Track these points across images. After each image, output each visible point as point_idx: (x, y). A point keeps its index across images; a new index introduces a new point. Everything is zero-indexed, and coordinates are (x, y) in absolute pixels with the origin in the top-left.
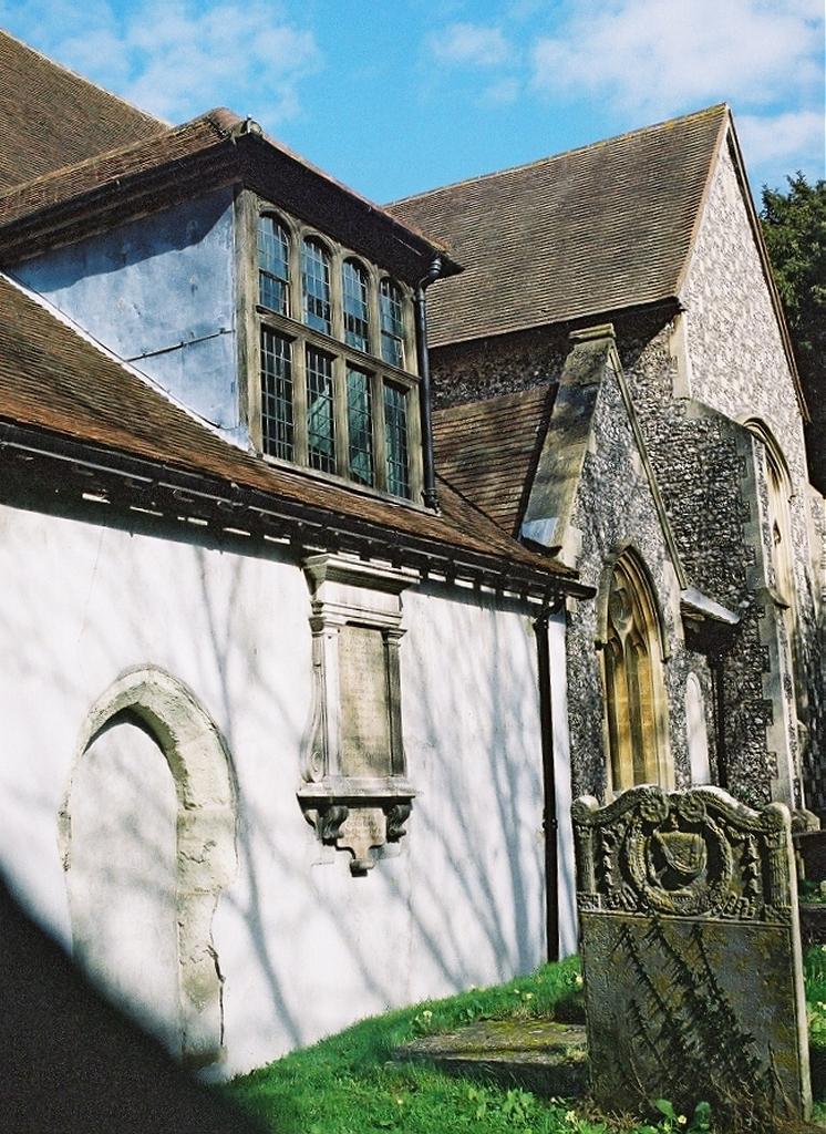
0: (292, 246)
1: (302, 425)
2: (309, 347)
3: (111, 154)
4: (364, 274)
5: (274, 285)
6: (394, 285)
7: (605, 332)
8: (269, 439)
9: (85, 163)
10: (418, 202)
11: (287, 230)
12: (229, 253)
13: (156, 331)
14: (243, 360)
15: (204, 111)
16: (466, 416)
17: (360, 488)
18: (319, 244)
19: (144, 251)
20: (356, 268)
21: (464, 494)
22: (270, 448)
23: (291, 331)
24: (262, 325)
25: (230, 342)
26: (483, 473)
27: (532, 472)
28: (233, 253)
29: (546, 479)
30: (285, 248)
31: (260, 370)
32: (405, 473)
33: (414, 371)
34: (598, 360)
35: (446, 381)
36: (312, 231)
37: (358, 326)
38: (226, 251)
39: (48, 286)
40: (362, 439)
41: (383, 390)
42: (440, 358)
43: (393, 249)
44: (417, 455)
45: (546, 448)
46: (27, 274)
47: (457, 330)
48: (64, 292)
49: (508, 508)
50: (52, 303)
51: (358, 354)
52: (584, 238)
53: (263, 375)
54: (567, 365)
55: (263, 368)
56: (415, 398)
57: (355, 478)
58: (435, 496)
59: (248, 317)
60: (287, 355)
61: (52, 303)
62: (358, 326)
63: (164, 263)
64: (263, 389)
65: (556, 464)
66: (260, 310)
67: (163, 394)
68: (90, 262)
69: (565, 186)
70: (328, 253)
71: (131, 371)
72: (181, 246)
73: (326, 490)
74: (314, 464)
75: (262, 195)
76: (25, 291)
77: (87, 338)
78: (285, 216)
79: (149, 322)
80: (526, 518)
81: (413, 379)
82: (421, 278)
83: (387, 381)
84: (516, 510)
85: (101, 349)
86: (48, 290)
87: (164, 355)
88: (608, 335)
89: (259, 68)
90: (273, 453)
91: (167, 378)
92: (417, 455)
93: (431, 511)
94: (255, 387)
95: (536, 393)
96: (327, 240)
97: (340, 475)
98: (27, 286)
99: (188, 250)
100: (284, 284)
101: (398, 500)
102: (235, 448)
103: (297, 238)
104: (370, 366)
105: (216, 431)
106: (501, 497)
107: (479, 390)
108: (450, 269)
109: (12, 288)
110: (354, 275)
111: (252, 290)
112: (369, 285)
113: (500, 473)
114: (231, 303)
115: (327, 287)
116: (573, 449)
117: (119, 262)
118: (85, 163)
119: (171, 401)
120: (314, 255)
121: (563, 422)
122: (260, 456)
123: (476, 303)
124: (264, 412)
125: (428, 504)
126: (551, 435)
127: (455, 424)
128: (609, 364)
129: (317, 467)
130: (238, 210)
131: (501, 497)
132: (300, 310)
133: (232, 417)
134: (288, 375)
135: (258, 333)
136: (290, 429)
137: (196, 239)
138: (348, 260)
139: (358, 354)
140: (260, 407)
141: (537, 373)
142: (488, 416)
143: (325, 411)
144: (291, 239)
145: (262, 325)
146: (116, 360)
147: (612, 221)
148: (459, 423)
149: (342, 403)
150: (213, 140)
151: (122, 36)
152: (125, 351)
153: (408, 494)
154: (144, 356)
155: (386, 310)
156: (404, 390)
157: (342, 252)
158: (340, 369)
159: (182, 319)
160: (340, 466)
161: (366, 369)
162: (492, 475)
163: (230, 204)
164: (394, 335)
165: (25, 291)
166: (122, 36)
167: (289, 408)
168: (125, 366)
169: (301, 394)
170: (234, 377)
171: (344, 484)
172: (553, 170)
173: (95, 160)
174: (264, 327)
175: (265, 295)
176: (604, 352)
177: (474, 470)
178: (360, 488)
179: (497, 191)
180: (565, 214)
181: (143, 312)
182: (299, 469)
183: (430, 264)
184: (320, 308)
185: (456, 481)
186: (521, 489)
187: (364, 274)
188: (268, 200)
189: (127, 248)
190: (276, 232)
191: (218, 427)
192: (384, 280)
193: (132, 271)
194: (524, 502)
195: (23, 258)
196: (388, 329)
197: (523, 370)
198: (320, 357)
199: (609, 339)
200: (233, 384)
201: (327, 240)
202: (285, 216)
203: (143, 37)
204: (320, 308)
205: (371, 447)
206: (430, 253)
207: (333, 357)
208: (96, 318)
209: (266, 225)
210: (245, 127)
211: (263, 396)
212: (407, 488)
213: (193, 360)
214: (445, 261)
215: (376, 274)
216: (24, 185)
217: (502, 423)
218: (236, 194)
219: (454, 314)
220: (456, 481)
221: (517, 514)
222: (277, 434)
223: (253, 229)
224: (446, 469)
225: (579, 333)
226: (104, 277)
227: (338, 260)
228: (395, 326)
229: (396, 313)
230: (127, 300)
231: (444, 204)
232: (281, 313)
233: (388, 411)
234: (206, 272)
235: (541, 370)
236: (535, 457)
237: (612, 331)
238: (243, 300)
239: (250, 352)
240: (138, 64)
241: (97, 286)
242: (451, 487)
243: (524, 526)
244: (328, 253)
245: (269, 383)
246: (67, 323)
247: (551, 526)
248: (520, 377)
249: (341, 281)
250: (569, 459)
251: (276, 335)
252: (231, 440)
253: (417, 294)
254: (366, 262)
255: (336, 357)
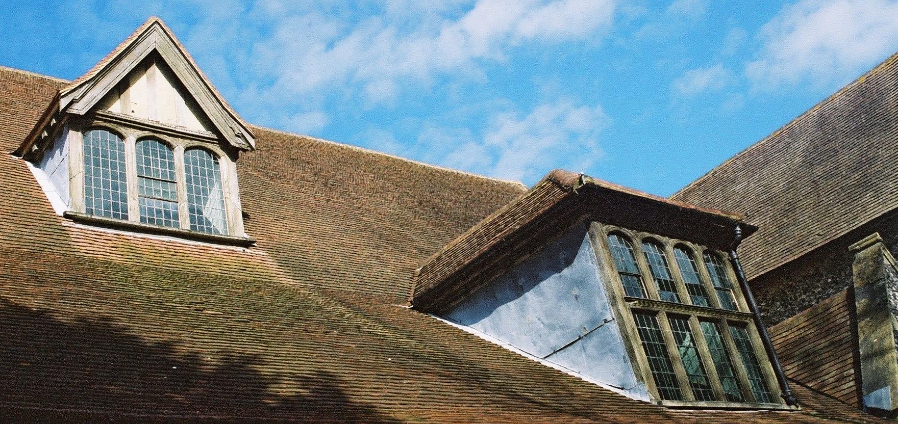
0: (635, 250)
1: (680, 370)
2: (669, 315)
3: (489, 219)
4: (690, 253)
5: (632, 280)
6: (713, 254)
7: (874, 239)
8: (661, 388)
9: (473, 229)
10: (699, 185)
11: (629, 239)
12: (596, 267)
13: (558, 332)
14: (626, 338)
15: (546, 174)
16: (792, 327)
17: (737, 405)
18: (654, 242)
19: (534, 280)
20: (683, 250)
21: (810, 385)
22: (665, 395)
23: (655, 308)
24: (632, 309)
25: (614, 327)
26: (819, 366)
27: (856, 356)
28: (596, 262)
29: (869, 357)
30: (631, 252)
31: (640, 342)
32: (763, 383)
33: (747, 310)
34: (877, 258)
35: (764, 304)
36: (647, 234)
37: (697, 290)
38: (592, 265)
39: (475, 318)
40: (725, 367)
41: (730, 331)
42: (756, 287)
43: (703, 229)
44: (768, 367)
45: (861, 337)
46: (458, 315)
47: (758, 266)
48: (486, 321)
49: (849, 385)
50: (480, 330)
51: (703, 310)
52: (829, 175)
53: (643, 344)
54: (855, 270)
55: (642, 340)
56: (753, 327)
57: (730, 399)
58: (792, 395)
59: (621, 307)
60: (656, 325)
61: (480, 330)
62: (697, 290)
63: (550, 285)
64: (647, 354)
65: (872, 346)
66: (628, 300)
67: (577, 375)
68: (499, 296)
69: (801, 145)
70: (661, 246)
71: (549, 365)
72: (559, 270)
73: (715, 415)
74: (699, 398)
75: (604, 222)
76: (460, 327)
77: (511, 349)
78: (624, 230)
79: (552, 327)
80: (865, 393)
81: (747, 315)
82: (731, 243)
83: (731, 323)
84: (854, 388)
85: (524, 354)
86: (475, 322)
87: (569, 348)
88: (878, 241)
89: (573, 135)
90: (667, 398)
91: (575, 363)
92: (768, 367)
93: (793, 407)
94: (641, 355)
95: (839, 298)
96: (657, 237)
97: (719, 399)
98: (461, 323)
99: (565, 272)
100: (637, 276)
101: (768, 406)
102: (641, 402)
103: (637, 242)
104: (717, 316)
105: (622, 393)
106: (840, 379)
107: (790, 304)
108: (749, 230)
109: (451, 327)
110: (683, 255)
111: (618, 286)
112: (695, 257)
113: (832, 363)
114: (606, 300)
115: (668, 270)
116: (880, 332)
117: (519, 291)
118: (473, 229)
119: (584, 379)
120: (652, 250)
121: (866, 313)
122: (660, 404)
123: (767, 243)
124: (652, 370)
125: (789, 404)
126: (861, 324)
127: (784, 334)
128: (886, 261)
129: (701, 399)
130: (592, 236)
131: (840, 379)
132: (653, 288)
133: (633, 380)
134: (661, 340)
135: (631, 317)
136: (674, 377)
137: (569, 262)
138: (676, 246)
139: (703, 310)
140: (648, 367)
141: (829, 280)
142: (807, 323)
143: (691, 351)
144: (633, 245)
145: (632, 309)
146: (536, 360)
147: (847, 158)
148: (787, 333)
149: (704, 347)
150: (559, 195)
151: (481, 143)
152: (540, 352)
153: (772, 399)
154: (555, 352)
155: (714, 272)
156: (745, 325)
157: (670, 243)
158: (694, 322)
159: (577, 318)
160: (717, 394)
161: (715, 318)
162: (826, 366)
163: (585, 234)
164: (724, 288)
165: (460, 327)
166: (481, 143)
167: (669, 362)
168: (544, 363)
169: (674, 350)
170: (622, 350)
171: (724, 406)
172: (791, 133)
173: (479, 225)
174: (634, 311)
175: (628, 289)
176: (879, 253)
177: (811, 364)
178: (737, 405)
179: (754, 161)
180: (809, 163)
181: (546, 322)
182: (690, 405)
183: (734, 233)
184: (668, 286)
185: (800, 377)
186: (852, 371)
187: (690, 253)
188: (609, 224)
189: (522, 281)
190: (621, 242)
191: (622, 389)
192: (705, 252)
193: (530, 295)
194: (858, 379)
195: (453, 304)
196: (718, 285)
197: (818, 281)
198: (679, 320)
199: (879, 244)
200: (624, 357)
201: (657, 237)
202: (624, 230)
203: (494, 139)
204: (668, 286)
205: (733, 370)
206: (731, 224)
207: (687, 317)
208: (514, 333)
209: (614, 240)
210: (581, 182)
211: (649, 359)
212: (769, 395)
213: (591, 344)
214: (743, 226)
215: (698, 250)
216: (437, 255)
217: (823, 322)
218: (588, 227)
219: (755, 257)
220: (800, 377)
221: (856, 391)
222: (666, 384)
223: (606, 246)
224: (790, 369)
225: (856, 246)
226: (511, 304)
227: (669, 248)
228: (723, 281)
229: (721, 273)
230: (532, 317)
231: (719, 180)
232: (643, 297)
233: (738, 344)
234: (581, 283)
235: (832, 277)
236: (855, 346)
237: (879, 237)
238: (614, 297)
239: (629, 330)
240: (495, 154)
241: (508, 311)
242: (798, 383)
243: (865, 398)
244: (661, 246)
245: (649, 349)
246: (494, 341)
247: (887, 392)
248: (818, 287)
249: (676, 262)
250: (881, 339)
251: (645, 313)
252: (636, 397)
253: (730, 255)
254: (689, 244)
255: (690, 316)
